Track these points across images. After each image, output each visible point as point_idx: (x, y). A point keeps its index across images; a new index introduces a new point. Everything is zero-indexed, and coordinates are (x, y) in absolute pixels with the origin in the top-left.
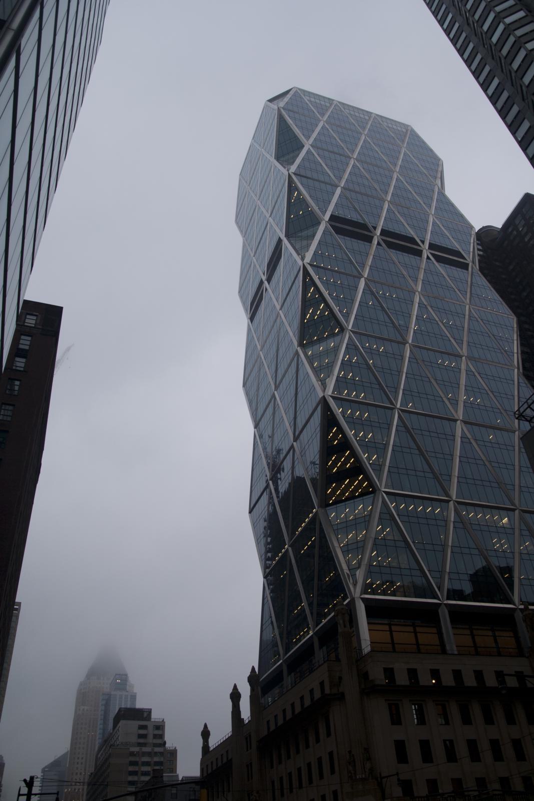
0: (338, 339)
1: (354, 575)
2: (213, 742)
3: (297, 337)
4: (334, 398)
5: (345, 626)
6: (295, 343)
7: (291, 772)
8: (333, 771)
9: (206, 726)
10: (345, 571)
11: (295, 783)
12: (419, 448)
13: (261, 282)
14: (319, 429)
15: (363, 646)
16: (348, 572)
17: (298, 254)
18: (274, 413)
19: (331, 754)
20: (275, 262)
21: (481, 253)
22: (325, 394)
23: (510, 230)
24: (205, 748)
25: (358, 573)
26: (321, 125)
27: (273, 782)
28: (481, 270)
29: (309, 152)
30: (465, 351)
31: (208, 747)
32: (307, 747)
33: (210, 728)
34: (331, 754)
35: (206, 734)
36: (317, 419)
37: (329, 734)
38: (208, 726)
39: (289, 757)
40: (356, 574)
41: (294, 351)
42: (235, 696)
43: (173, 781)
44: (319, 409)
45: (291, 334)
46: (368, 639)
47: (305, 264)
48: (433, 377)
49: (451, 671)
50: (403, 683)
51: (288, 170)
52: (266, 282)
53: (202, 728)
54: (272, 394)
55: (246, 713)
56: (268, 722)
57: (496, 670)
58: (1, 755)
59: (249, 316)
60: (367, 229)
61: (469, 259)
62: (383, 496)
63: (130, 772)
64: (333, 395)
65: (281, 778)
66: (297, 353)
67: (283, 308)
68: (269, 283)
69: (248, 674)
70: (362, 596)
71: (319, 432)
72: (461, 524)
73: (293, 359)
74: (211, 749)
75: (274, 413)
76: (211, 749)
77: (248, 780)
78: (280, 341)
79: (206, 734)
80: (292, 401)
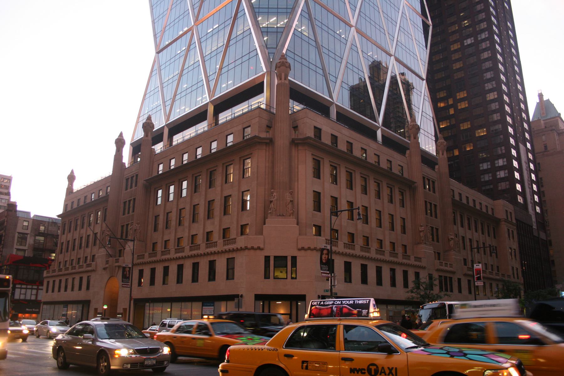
2: (78, 186)
9: (72, 172)
12: (323, 69)
24: (70, 191)
30: (353, 22)
31: (72, 190)
35: (71, 178)
42: (120, 143)
43: (340, 178)
48: (387, 31)
53: (69, 173)
58: (3, 178)
63: (63, 314)
65: (81, 238)
69: (117, 137)
74: (74, 191)
76: (74, 191)
79: (71, 178)
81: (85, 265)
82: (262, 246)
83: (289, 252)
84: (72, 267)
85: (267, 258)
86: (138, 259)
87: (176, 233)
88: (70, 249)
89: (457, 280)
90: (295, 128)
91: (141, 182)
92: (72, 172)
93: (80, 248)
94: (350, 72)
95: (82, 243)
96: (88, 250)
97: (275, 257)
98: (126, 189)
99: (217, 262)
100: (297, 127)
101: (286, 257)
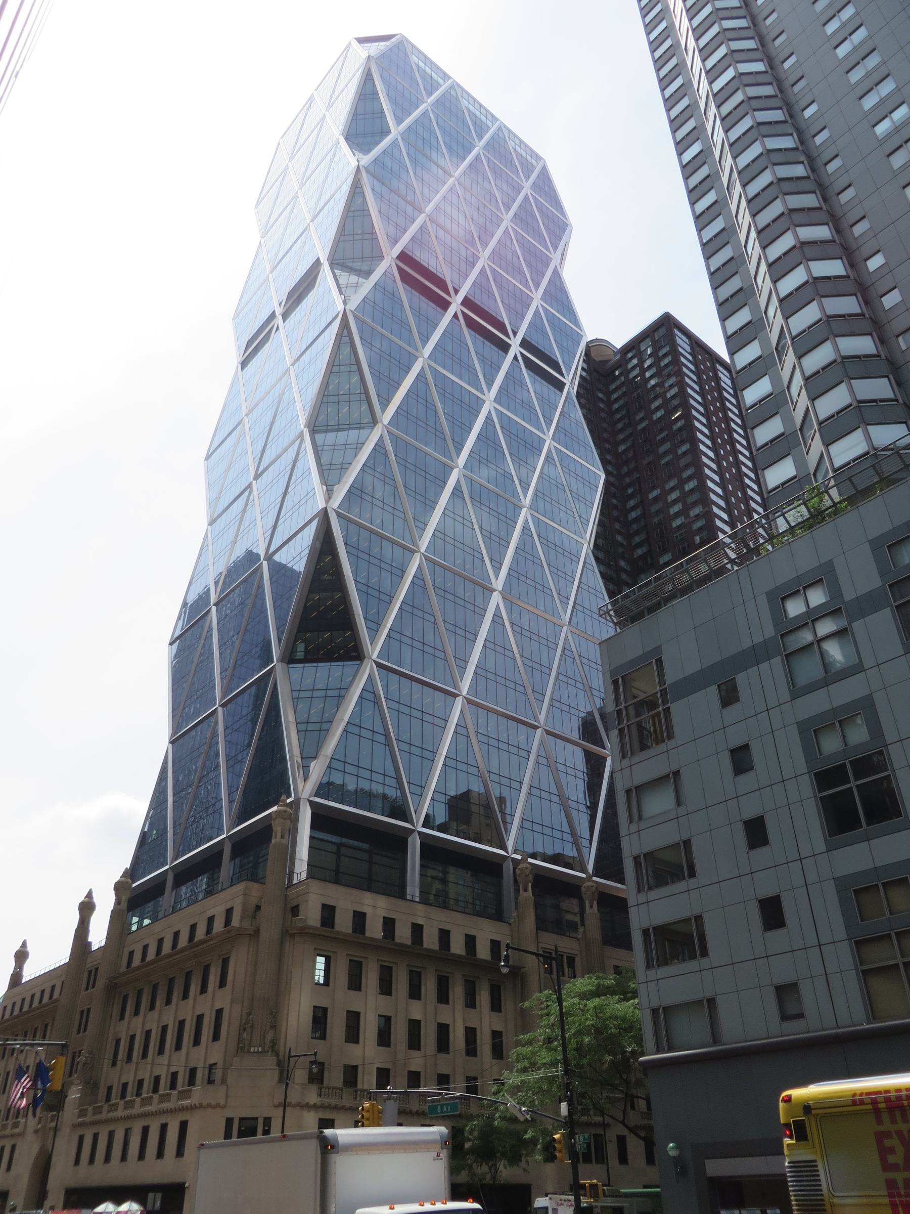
0: (366, 431)
1: (306, 768)
2: (30, 972)
3: (307, 412)
4: (339, 515)
5: (282, 837)
6: (302, 421)
7: (151, 1030)
8: (216, 1037)
9: (24, 944)
10: (295, 758)
11: (136, 1054)
13: (273, 316)
14: (307, 551)
15: (297, 870)
16: (300, 761)
17: (341, 293)
18: (244, 511)
19: (219, 1012)
20: (303, 291)
21: (584, 374)
22: (329, 505)
23: (630, 355)
24: (16, 979)
25: (312, 765)
26: (422, 108)
27: (118, 1041)
28: (578, 395)
29: (394, 143)
32: (185, 996)
33: (30, 948)
34: (219, 1012)
35: (21, 956)
36: (308, 536)
37: (222, 984)
38: (28, 945)
39: (152, 1007)
40: (309, 766)
41: (298, 432)
42: (87, 908)
44: (315, 524)
45: (299, 406)
46: (307, 860)
47: (348, 311)
49: (489, 943)
50: (343, 930)
51: (358, 161)
52: (280, 318)
53: (82, 898)
54: (247, 484)
55: (98, 936)
56: (131, 953)
57: (492, 938)
59: (241, 359)
60: (444, 288)
61: (567, 381)
62: (372, 666)
64: (339, 510)
65: (133, 1037)
66: (302, 433)
67: (297, 364)
68: (284, 320)
70: (312, 799)
71: (306, 557)
72: (384, 737)
73: (293, 442)
75: (244, 511)
77: (79, 1032)
78: (279, 411)
79: (21, 956)
80: (294, 485)
81: (122, 1103)
82: (222, 1102)
83: (260, 1113)
84: (126, 1102)
85: (229, 1121)
86: (125, 1108)
87: (135, 1073)
88: (120, 1057)
89: (615, 1140)
90: (295, 910)
91: (101, 983)
92: (90, 895)
93: (161, 1051)
94: (557, 712)
95: (149, 1045)
96: (164, 1059)
97: (241, 1119)
98: (87, 989)
99: (169, 1126)
100: (297, 906)
101: (256, 1119)
